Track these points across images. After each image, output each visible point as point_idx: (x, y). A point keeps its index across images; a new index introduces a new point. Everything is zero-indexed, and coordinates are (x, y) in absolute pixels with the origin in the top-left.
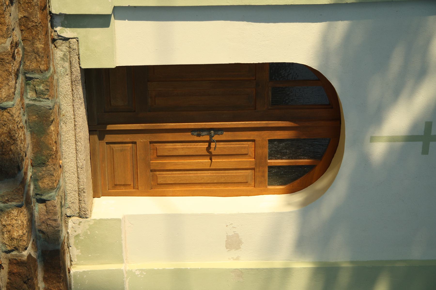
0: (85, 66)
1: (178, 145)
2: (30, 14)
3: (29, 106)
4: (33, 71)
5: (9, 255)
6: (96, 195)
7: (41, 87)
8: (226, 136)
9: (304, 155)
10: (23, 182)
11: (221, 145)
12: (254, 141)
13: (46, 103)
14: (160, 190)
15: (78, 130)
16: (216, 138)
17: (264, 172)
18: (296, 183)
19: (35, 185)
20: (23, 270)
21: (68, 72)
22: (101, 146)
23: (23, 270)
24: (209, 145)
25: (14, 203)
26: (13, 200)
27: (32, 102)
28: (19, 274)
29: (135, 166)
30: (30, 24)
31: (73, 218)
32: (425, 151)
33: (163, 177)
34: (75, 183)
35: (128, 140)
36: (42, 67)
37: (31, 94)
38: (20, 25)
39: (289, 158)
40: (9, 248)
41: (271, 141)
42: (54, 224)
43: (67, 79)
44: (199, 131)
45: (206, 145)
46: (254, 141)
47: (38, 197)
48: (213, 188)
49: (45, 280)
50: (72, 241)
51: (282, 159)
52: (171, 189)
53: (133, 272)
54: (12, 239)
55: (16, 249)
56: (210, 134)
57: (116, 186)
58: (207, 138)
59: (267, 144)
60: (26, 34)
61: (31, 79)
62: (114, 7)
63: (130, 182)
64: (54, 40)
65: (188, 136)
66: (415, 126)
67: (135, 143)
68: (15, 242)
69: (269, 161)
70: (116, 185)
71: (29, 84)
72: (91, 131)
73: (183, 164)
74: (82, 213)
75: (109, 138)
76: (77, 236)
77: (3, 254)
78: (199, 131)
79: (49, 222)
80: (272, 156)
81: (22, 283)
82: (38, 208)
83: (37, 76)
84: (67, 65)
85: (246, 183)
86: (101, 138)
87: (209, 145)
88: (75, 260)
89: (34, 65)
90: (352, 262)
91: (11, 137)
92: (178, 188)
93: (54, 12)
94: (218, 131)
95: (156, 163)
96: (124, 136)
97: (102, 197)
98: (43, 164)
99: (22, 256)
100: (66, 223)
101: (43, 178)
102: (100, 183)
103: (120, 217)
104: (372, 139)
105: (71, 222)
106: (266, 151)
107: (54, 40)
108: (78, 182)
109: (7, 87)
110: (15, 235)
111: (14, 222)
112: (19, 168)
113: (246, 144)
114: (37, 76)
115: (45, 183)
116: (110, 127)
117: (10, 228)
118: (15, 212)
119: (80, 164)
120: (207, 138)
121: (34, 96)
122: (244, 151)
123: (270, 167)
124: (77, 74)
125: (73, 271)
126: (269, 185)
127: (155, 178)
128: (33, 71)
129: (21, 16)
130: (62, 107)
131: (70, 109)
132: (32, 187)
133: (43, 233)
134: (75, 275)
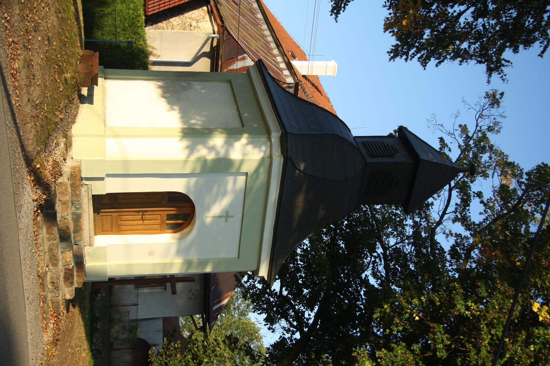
0: (93, 194)
1: (130, 216)
2: (75, 182)
3: (73, 213)
4: (75, 201)
5: (65, 267)
6: (95, 234)
7: (78, 206)
8: (149, 213)
9: (181, 219)
10: (71, 242)
11: (147, 216)
12: (160, 215)
13: (79, 212)
14: (122, 232)
15: (90, 216)
16: (145, 214)
17: (164, 225)
18: (177, 229)
19: (74, 239)
20: (70, 272)
21: (87, 195)
22: (98, 217)
23: (70, 272)
24: (142, 216)
25: (68, 250)
26: (67, 248)
27: (74, 211)
28: (69, 273)
29: (112, 224)
30: (75, 186)
31: (87, 246)
32: (226, 221)
33: (123, 228)
34: (88, 234)
35: (109, 215)
36: (78, 200)
37: (74, 208)
38: (71, 186)
39: (175, 220)
40: (65, 265)
41: (167, 215)
42: (81, 252)
43: (87, 198)
44: (138, 212)
45: (141, 216)
46: (160, 215)
47: (75, 243)
48: (144, 231)
49: (77, 272)
50: (86, 255)
51: (172, 220)
52: (126, 232)
53: (100, 80)
54: (66, 262)
55: (68, 265)
56: (143, 213)
57: (103, 231)
58: (142, 214)
59: (166, 216)
60: (73, 189)
61: (74, 203)
62: (107, 174)
63: (109, 229)
64: (82, 185)
65: (134, 213)
66: (222, 211)
67: (112, 216)
68: (67, 263)
69: (167, 222)
70: (104, 231)
71: (73, 205)
72: (94, 212)
73: (132, 223)
74: (91, 245)
75: (101, 214)
76: (89, 253)
77: (63, 266)
78: (138, 212)
79: (79, 252)
80: (167, 220)
81: (69, 276)
82: (75, 247)
83: (76, 202)
84: (87, 193)
85: (157, 229)
86: (98, 214)
87: (142, 216)
88: (87, 261)
89: (75, 199)
90: (198, 259)
91: (67, 228)
92: (129, 232)
93: (82, 177)
94: (145, 211)
95: (120, 223)
96: (108, 213)
97: (98, 235)
98: (78, 232)
99: (70, 267)
100: (84, 248)
101: (77, 237)
102: (97, 229)
103: (106, 246)
104: (206, 217)
105: (86, 248)
106: (166, 218)
107: (82, 185)
108: (90, 234)
109: (67, 212)
110: (68, 260)
111: (67, 256)
112: (70, 238)
113: (157, 216)
114: (76, 202)
115: (78, 238)
116: (102, 211)
117: (66, 258)
118: (68, 253)
119: (90, 228)
120: (142, 214)
121: (75, 209)
122: (156, 218)
123: (167, 224)
124: (91, 197)
125: (86, 265)
126: (166, 230)
127: (120, 228)
128: (75, 201)
129: (71, 183)
130: (84, 208)
131: (87, 208)
132: (73, 240)
133: (10, 100)
134: (88, 267)
